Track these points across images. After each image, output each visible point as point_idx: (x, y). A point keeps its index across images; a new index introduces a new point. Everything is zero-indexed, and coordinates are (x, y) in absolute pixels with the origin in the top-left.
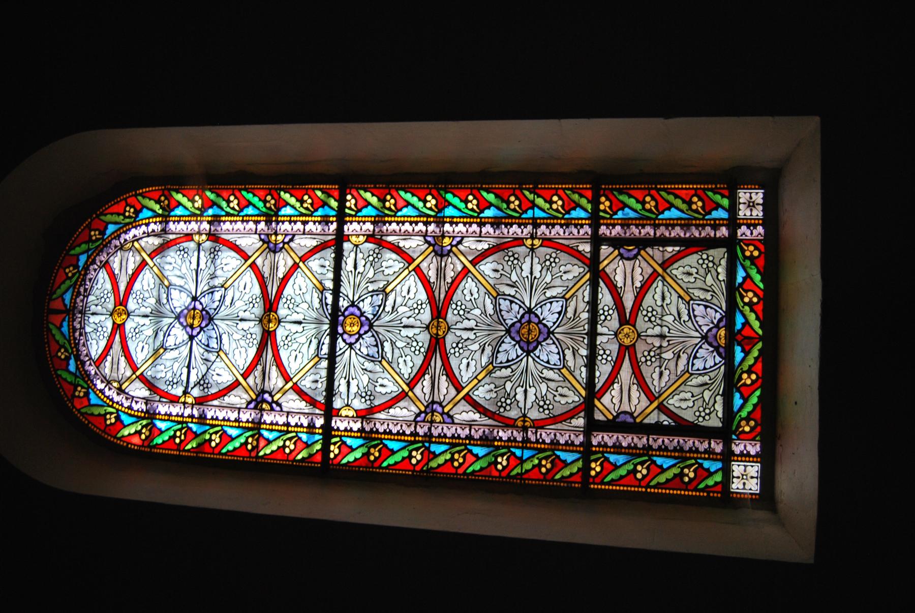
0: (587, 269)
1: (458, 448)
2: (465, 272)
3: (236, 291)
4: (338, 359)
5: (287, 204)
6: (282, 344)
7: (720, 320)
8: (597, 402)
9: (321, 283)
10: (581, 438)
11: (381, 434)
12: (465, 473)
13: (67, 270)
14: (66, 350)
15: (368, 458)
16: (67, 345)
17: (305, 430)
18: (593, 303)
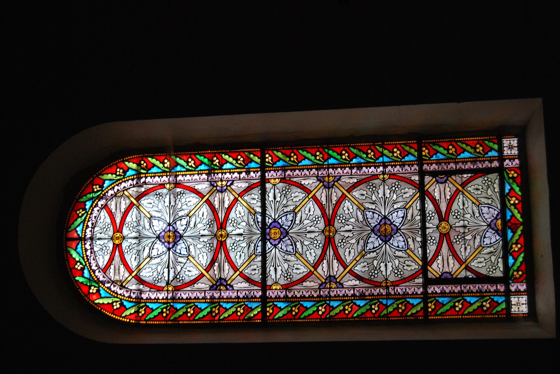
0: (417, 190)
4: (268, 255)
5: (227, 162)
7: (497, 215)
8: (429, 268)
10: (421, 290)
12: (352, 317)
13: (78, 212)
18: (423, 210)
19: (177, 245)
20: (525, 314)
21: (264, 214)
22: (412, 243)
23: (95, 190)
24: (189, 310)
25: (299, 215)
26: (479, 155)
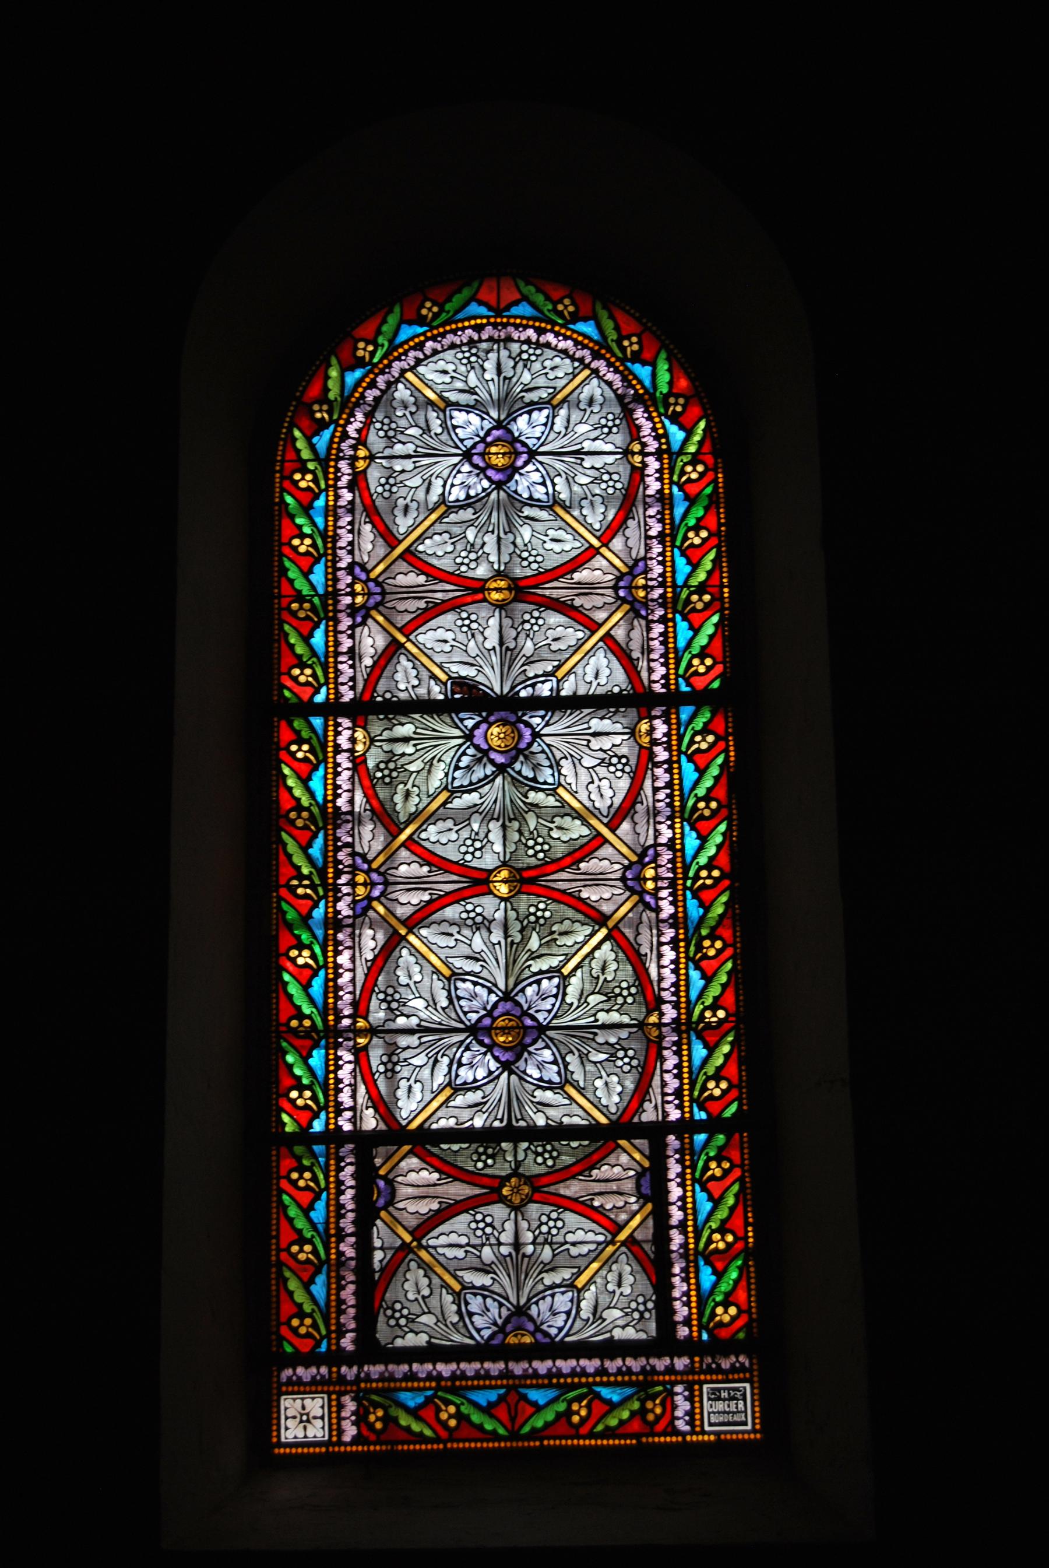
0: (614, 1118)
1: (321, 1177)
2: (593, 626)
3: (561, 1111)
6: (469, 907)
7: (546, 1334)
8: (406, 1148)
9: (568, 673)
11: (337, 1176)
12: (281, 1191)
13: (567, 301)
14: (436, 316)
15: (294, 878)
16: (444, 317)
17: (331, 503)
18: (557, 1133)
19: (478, 475)
20: (279, 1436)
21: (557, 704)
22: (471, 1103)
23: (626, 343)
24: (308, 1321)
25: (544, 515)
26: (698, 1086)
